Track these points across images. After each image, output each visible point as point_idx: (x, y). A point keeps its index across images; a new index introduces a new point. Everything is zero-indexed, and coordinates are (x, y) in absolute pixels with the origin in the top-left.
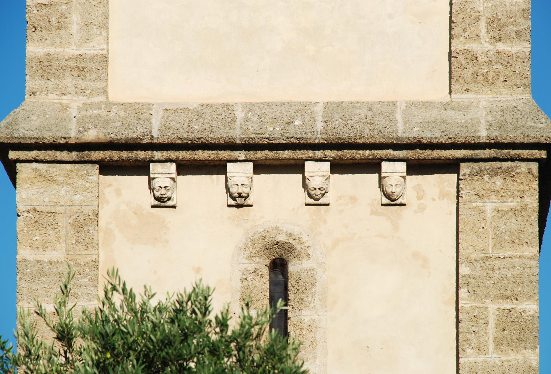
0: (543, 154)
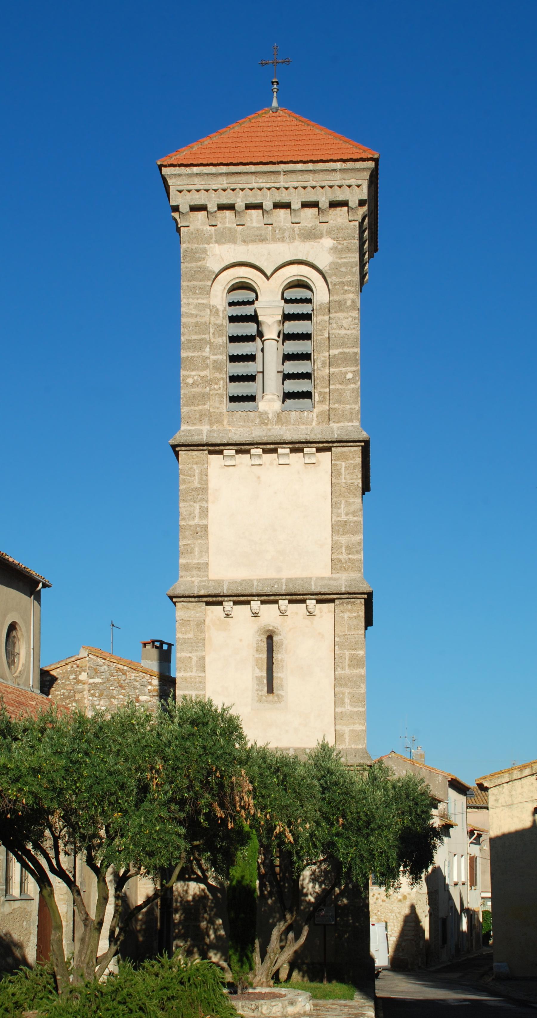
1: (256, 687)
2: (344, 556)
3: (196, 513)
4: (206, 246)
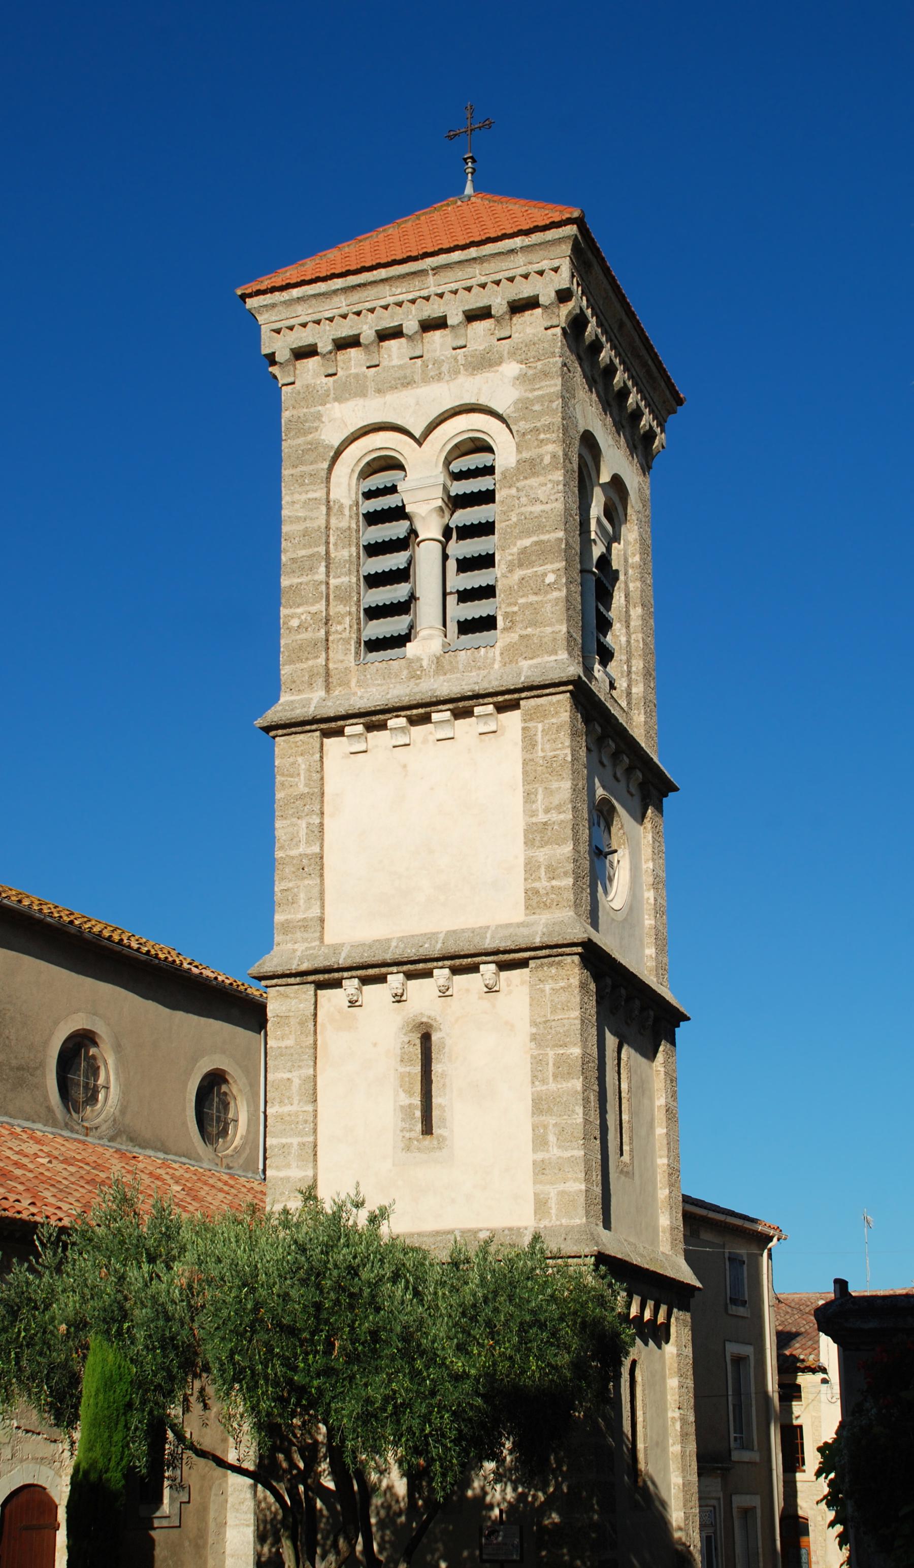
0: (579, 950)
1: (401, 1125)
2: (543, 884)
3: (301, 835)
4: (320, 408)
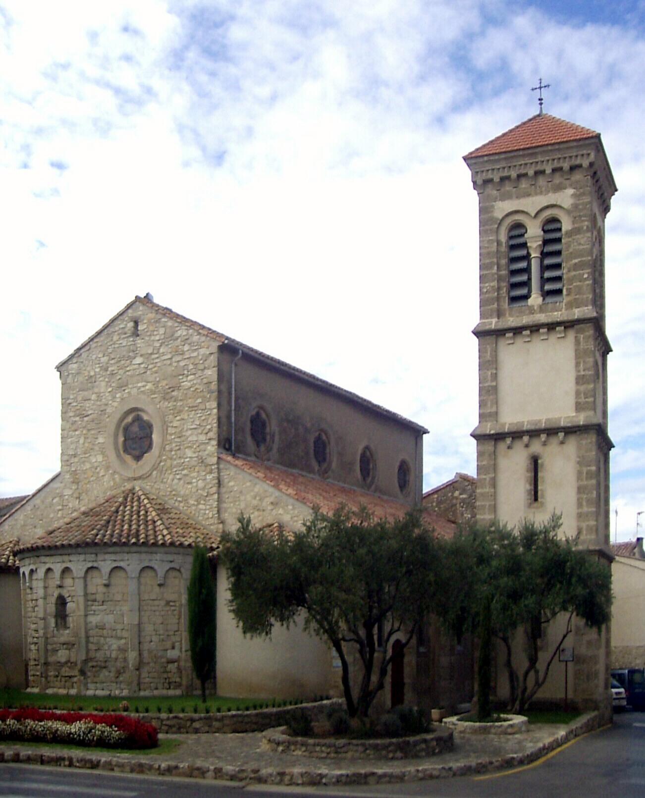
2: (582, 400)
